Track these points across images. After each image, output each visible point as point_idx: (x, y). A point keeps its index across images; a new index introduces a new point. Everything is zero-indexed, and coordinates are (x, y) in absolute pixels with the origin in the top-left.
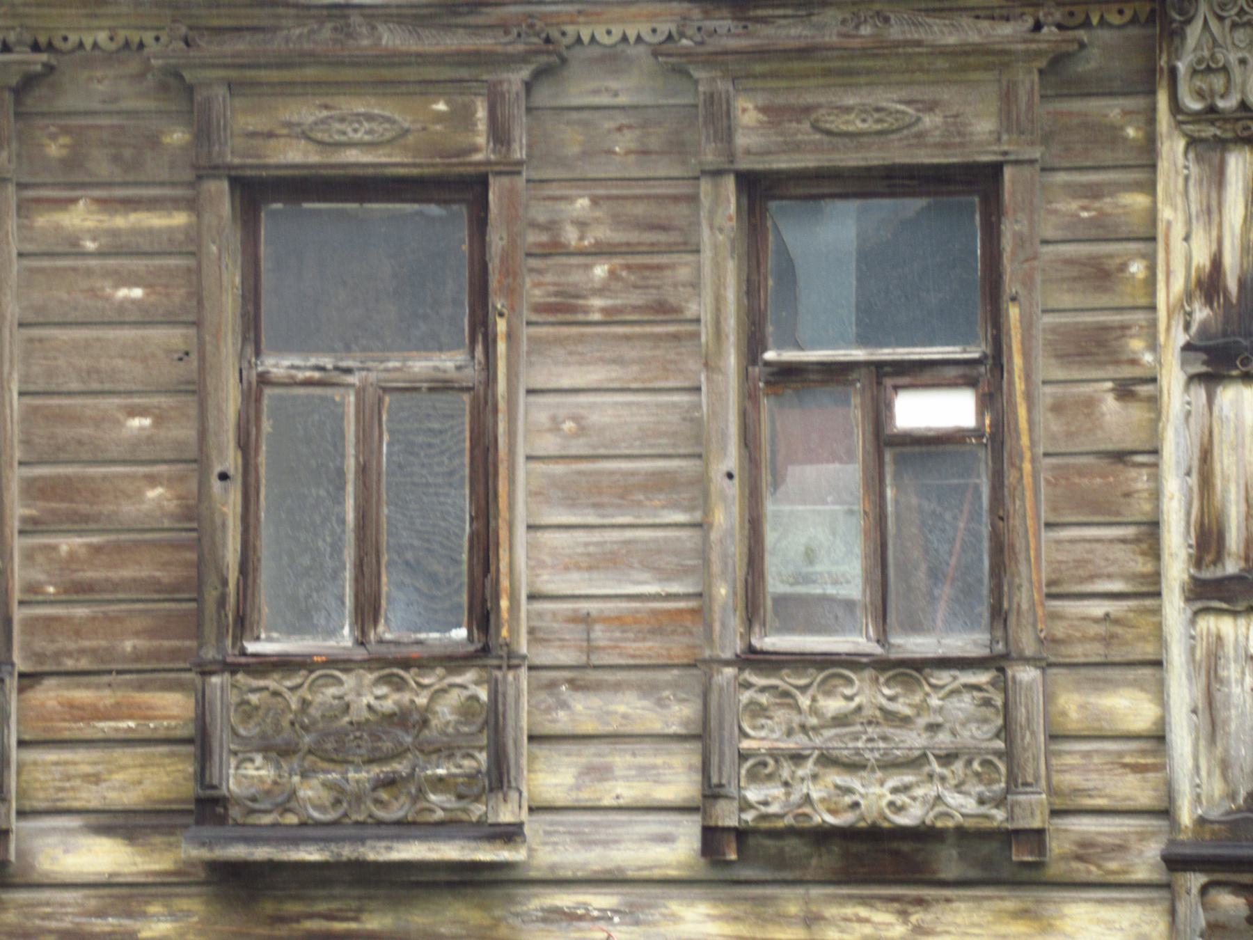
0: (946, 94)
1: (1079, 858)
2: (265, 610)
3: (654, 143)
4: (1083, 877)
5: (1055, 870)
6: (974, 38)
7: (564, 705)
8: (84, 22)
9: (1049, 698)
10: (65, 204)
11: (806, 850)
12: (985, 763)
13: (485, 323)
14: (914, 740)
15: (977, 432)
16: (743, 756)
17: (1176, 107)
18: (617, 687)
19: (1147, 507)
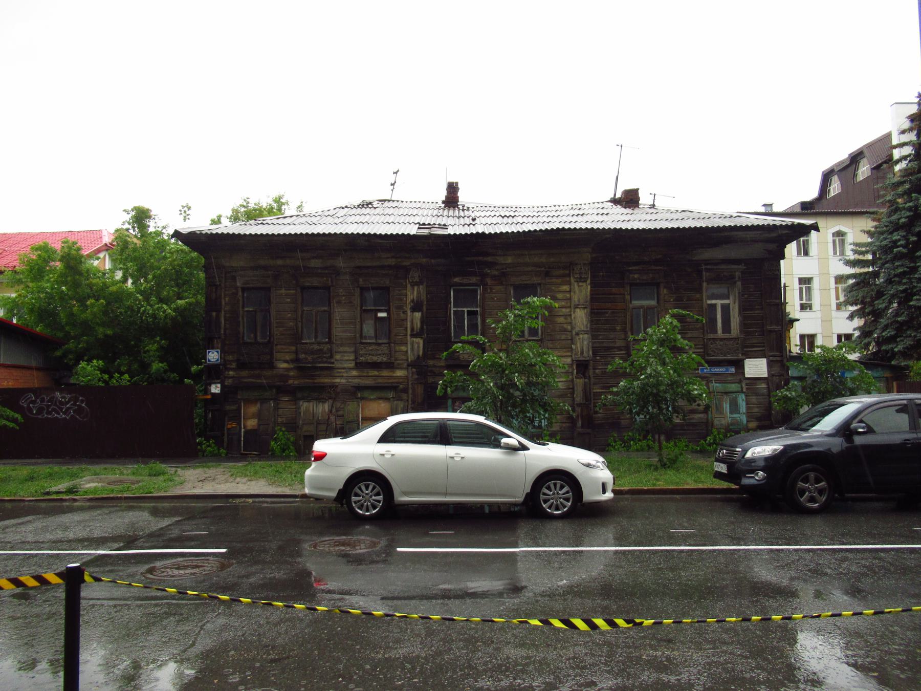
10: (280, 290)
14: (380, 352)
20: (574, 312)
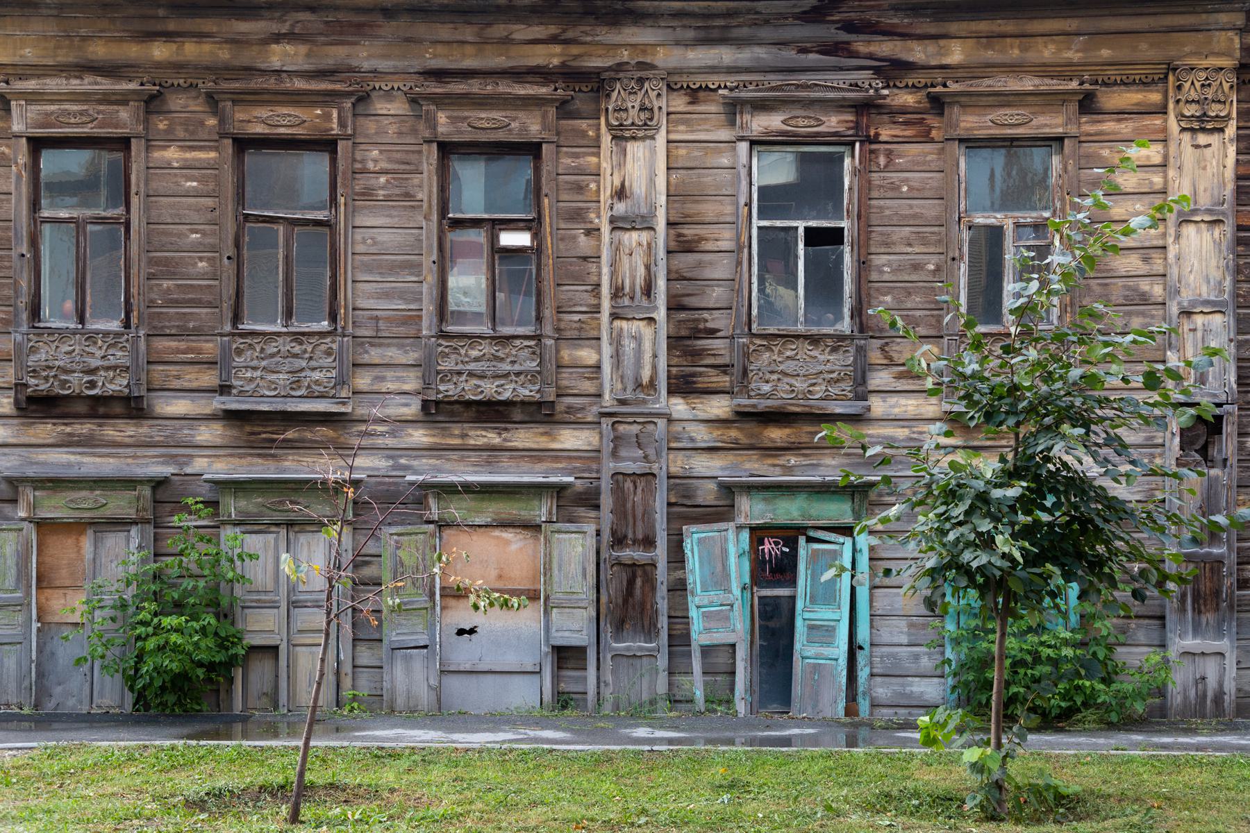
0: (521, 114)
1: (567, 413)
2: (246, 312)
3: (404, 129)
4: (569, 420)
5: (558, 417)
6: (531, 92)
7: (367, 352)
8: (174, 75)
9: (558, 351)
10: (165, 148)
11: (461, 409)
12: (532, 376)
13: (336, 199)
14: (506, 367)
15: (531, 248)
16: (438, 373)
17: (608, 124)
18: (389, 345)
19: (596, 278)
20: (1178, 237)
